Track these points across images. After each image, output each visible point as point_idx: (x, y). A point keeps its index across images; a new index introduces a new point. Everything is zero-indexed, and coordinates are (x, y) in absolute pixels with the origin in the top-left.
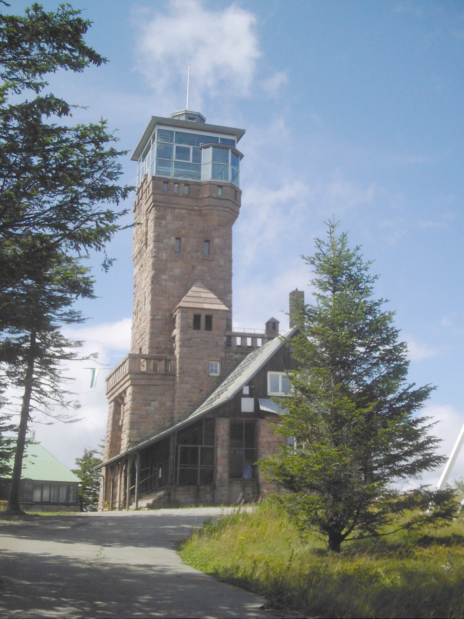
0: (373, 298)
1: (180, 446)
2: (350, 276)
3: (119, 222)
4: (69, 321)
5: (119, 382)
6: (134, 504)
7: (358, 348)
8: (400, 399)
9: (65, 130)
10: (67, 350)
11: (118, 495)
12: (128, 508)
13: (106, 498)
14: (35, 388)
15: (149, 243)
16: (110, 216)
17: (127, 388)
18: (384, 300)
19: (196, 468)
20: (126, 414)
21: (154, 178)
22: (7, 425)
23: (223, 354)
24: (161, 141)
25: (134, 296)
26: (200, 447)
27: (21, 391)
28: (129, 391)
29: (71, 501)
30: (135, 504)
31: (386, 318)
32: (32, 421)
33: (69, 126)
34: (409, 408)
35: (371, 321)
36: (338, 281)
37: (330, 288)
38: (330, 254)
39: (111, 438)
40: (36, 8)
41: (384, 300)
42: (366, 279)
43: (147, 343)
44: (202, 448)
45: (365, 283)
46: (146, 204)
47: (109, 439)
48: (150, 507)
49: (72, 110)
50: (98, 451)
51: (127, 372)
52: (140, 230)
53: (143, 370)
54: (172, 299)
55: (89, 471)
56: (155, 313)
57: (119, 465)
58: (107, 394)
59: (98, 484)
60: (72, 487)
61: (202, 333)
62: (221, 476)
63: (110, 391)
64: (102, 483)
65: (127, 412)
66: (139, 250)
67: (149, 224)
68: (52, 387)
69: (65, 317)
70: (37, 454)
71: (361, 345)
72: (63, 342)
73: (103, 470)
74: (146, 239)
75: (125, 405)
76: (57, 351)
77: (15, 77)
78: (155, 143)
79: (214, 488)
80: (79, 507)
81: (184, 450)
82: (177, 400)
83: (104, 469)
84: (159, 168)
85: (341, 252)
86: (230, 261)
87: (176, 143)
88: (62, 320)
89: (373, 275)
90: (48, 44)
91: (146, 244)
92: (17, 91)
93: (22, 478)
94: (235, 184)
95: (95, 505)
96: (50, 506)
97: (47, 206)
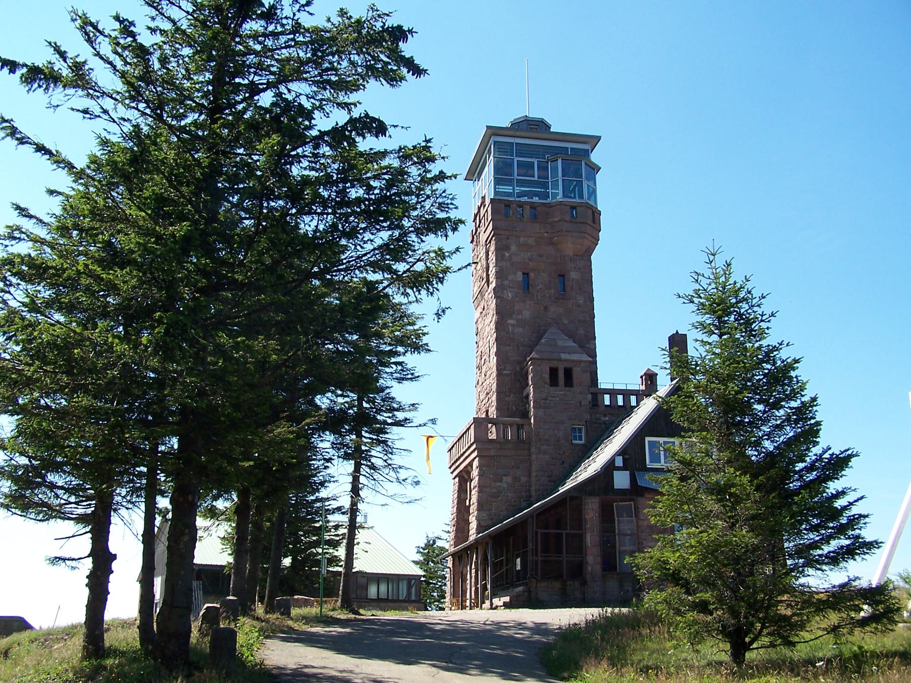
0: (769, 341)
1: (540, 531)
2: (740, 315)
3: (451, 262)
4: (400, 380)
5: (464, 453)
6: (488, 603)
7: (755, 406)
8: (811, 468)
9: (384, 154)
10: (400, 415)
11: (468, 591)
12: (481, 607)
13: (454, 595)
14: (365, 462)
15: (491, 280)
16: (441, 254)
17: (473, 460)
18: (785, 343)
19: (560, 559)
20: (473, 492)
23: (587, 417)
25: (476, 345)
26: (564, 532)
27: (350, 466)
28: (476, 463)
29: (413, 598)
31: (790, 366)
33: (389, 149)
34: (825, 478)
35: (769, 370)
36: (725, 322)
38: (712, 289)
39: (457, 521)
40: (342, 13)
41: (785, 343)
43: (494, 403)
44: (567, 534)
47: (453, 522)
48: (507, 606)
49: (391, 131)
51: (472, 440)
54: (521, 348)
55: (433, 562)
56: (502, 367)
57: (468, 554)
58: (450, 468)
60: (413, 581)
61: (561, 391)
62: (592, 569)
63: (453, 464)
64: (448, 576)
68: (385, 461)
69: (395, 375)
70: (371, 542)
71: (759, 402)
72: (395, 406)
74: (488, 275)
75: (472, 480)
76: (389, 417)
78: (492, 157)
79: (584, 583)
80: (422, 605)
81: (546, 537)
82: (534, 474)
83: (450, 559)
89: (768, 312)
90: (359, 55)
91: (488, 281)
93: (354, 570)
94: (592, 203)
95: (442, 603)
97: (369, 247)
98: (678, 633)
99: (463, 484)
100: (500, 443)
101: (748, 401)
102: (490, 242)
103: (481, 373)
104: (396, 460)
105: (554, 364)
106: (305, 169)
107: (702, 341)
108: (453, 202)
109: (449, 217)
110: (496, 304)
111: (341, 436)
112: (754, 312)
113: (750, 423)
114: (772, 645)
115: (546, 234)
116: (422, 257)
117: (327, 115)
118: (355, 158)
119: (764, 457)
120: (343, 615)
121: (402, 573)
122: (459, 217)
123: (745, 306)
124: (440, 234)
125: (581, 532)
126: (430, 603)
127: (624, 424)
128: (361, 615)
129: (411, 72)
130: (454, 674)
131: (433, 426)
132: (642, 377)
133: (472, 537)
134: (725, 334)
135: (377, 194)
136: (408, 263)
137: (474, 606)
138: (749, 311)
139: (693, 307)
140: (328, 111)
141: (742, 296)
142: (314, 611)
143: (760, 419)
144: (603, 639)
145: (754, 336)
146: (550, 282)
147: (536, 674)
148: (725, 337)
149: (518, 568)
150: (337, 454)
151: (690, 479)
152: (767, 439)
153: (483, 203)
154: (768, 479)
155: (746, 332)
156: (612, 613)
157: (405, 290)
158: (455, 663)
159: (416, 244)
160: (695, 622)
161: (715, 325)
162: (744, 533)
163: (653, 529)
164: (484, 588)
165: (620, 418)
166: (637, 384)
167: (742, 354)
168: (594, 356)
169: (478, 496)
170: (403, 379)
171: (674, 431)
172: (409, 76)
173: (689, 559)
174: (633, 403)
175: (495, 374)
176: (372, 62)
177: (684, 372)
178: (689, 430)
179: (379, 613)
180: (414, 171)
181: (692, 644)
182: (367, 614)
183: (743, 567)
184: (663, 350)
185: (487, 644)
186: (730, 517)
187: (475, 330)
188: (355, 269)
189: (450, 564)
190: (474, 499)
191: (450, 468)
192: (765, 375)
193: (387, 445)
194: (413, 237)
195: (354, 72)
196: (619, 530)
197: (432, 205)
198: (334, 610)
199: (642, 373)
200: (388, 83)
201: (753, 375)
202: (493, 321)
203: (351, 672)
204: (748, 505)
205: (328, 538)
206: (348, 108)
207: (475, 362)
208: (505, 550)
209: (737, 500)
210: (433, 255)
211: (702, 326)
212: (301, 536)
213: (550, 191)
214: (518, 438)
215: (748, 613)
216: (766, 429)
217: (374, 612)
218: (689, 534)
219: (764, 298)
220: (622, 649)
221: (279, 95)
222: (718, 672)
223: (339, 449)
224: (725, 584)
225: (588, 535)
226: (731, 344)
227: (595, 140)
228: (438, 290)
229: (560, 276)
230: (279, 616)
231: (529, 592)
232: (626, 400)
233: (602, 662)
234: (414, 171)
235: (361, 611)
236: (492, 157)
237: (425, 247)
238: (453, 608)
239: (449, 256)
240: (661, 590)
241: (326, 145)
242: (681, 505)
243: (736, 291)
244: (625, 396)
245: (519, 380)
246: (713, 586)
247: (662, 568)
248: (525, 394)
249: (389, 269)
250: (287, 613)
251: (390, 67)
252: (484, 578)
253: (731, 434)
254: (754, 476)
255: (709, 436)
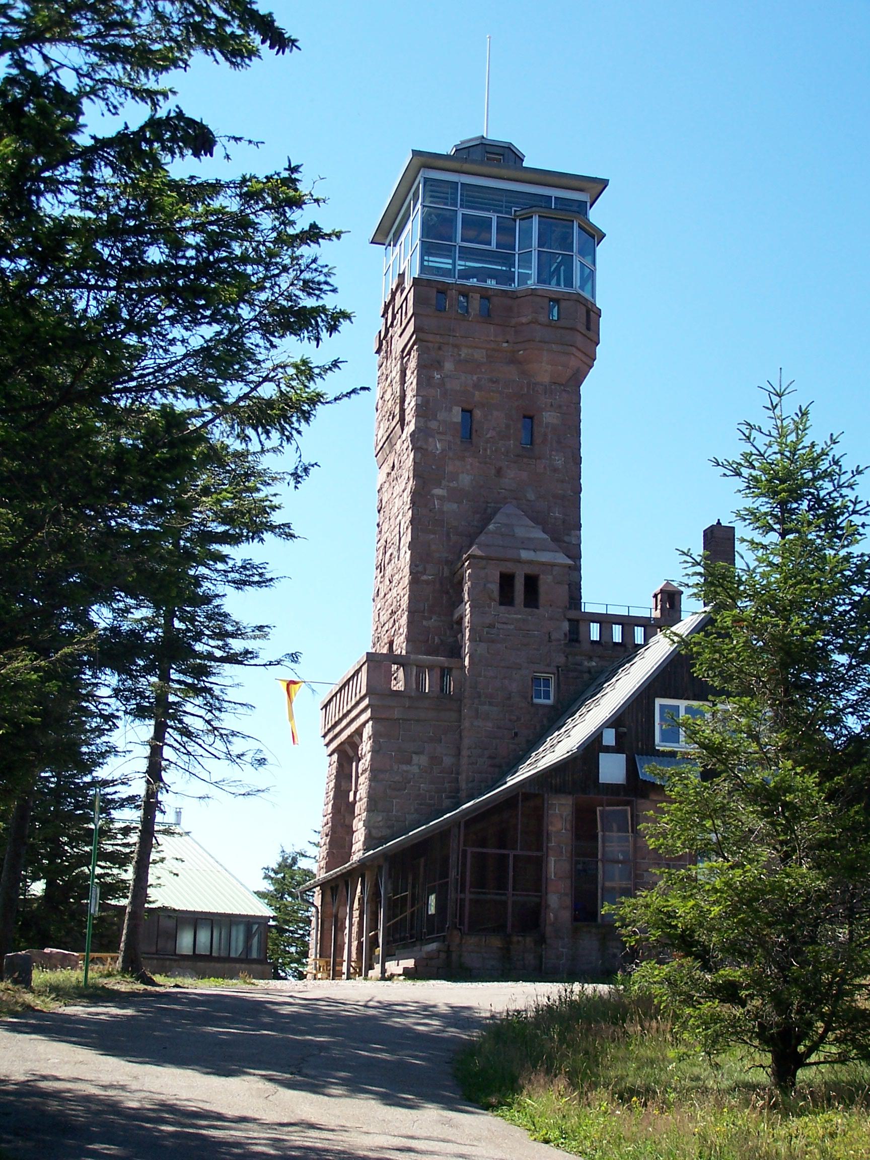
1: (470, 850)
2: (819, 500)
3: (325, 385)
4: (240, 584)
5: (349, 712)
7: (836, 657)
9: (216, 188)
10: (237, 645)
12: (366, 975)
13: (323, 953)
14: (172, 723)
15: (407, 419)
16: (305, 370)
19: (503, 898)
20: (362, 779)
21: (416, 282)
22: (124, 796)
23: (561, 659)
24: (431, 202)
25: (377, 530)
26: (512, 853)
27: (146, 729)
28: (368, 731)
30: (378, 967)
32: (167, 791)
33: (225, 178)
35: (862, 596)
36: (792, 511)
37: (776, 527)
38: (772, 456)
39: (333, 829)
42: (852, 506)
43: (404, 630)
45: (850, 515)
46: (400, 336)
47: (326, 829)
48: (409, 974)
50: (307, 854)
51: (364, 692)
52: (389, 392)
53: (395, 689)
56: (420, 569)
58: (324, 736)
59: (308, 921)
60: (255, 927)
61: (518, 613)
62: (556, 918)
63: (329, 730)
64: (313, 919)
65: (364, 776)
66: (387, 434)
67: (407, 378)
68: (208, 722)
69: (232, 575)
71: (842, 650)
72: (229, 628)
73: (316, 895)
74: (402, 410)
76: (218, 647)
77: (106, 76)
78: (419, 206)
79: (541, 940)
82: (465, 752)
84: (428, 261)
85: (796, 450)
86: (578, 460)
87: (462, 206)
88: (229, 582)
92: (111, 108)
94: (587, 295)
95: (303, 964)
96: (212, 964)
97: (179, 350)
98: (686, 1036)
99: (345, 764)
100: (410, 697)
101: (823, 649)
102: (409, 354)
103: (383, 576)
104: (227, 721)
105: (508, 568)
106: (72, 206)
107: (752, 542)
108: (329, 279)
109: (324, 307)
110: (414, 459)
111: (132, 677)
112: (841, 496)
113: (824, 685)
114: (842, 1059)
115: (505, 345)
116: (273, 374)
117: (114, 110)
118: (160, 192)
119: (845, 742)
120: (124, 985)
121: (237, 912)
122: (341, 307)
123: (828, 486)
124: (306, 334)
125: (539, 854)
126: (283, 964)
127: (621, 673)
128: (154, 984)
129: (268, 43)
130: (303, 1093)
131: (293, 665)
132: (655, 596)
133: (356, 856)
134: (790, 531)
135: (192, 258)
136: (247, 383)
137: (356, 973)
138: (833, 495)
139: (740, 483)
140: (116, 103)
141: (823, 468)
142: (73, 976)
143: (842, 679)
144: (562, 1040)
145: (839, 537)
146: (508, 427)
147: (444, 1096)
148: (791, 537)
149: (432, 910)
150: (123, 708)
151: (718, 775)
152: (852, 714)
153: (400, 285)
154: (849, 780)
155: (826, 530)
156: (582, 992)
157: (243, 431)
158: (306, 1076)
159: (263, 351)
160: (716, 1019)
161: (776, 516)
162: (805, 871)
163: (657, 859)
164: (373, 942)
165: (616, 664)
166: (647, 608)
167: (816, 567)
168: (576, 556)
169: (370, 786)
170: (245, 583)
171: (700, 691)
172: (265, 49)
173: (709, 911)
174: (639, 638)
175: (406, 581)
176: (198, 19)
177: (718, 594)
178: (719, 693)
179: (188, 981)
180: (266, 221)
181: (709, 1054)
182: (165, 983)
183: (799, 927)
184: (684, 553)
185: (365, 1042)
186: (782, 843)
187: (377, 504)
188: (153, 390)
189: (317, 900)
190: (363, 791)
191: (324, 736)
192: (854, 605)
193: (212, 696)
194: (254, 339)
195: (163, 34)
196: (603, 855)
197: (292, 284)
198: (110, 975)
199: (657, 590)
200: (227, 59)
201: (834, 604)
202: (409, 490)
203: (123, 1088)
204: (814, 824)
205: (110, 849)
206: (152, 100)
207: (373, 558)
208: (410, 881)
209: (795, 814)
210: (291, 371)
211: (753, 516)
212: (65, 844)
213: (516, 270)
214: (442, 690)
215: (804, 1004)
216: (851, 696)
217: (179, 980)
218: (711, 869)
219: (859, 472)
220: (593, 1058)
221: (20, 64)
222: (747, 1103)
223: (127, 699)
224: (768, 953)
225: (552, 860)
226: (800, 549)
227: (599, 185)
228: (299, 432)
229: (525, 417)
230: (10, 986)
231: (448, 952)
232: (628, 633)
233: (556, 1081)
234: (266, 221)
235: (157, 978)
236: (419, 206)
237: (277, 356)
238: (319, 976)
239: (320, 374)
240: (661, 962)
241: (106, 165)
242: (702, 819)
243: (814, 460)
244: (626, 627)
245: (447, 593)
246: (749, 957)
247: (666, 924)
248: (456, 616)
249: (214, 394)
250: (24, 981)
251: (229, 30)
252: (374, 926)
253: (792, 703)
254: (827, 775)
255: (753, 704)
